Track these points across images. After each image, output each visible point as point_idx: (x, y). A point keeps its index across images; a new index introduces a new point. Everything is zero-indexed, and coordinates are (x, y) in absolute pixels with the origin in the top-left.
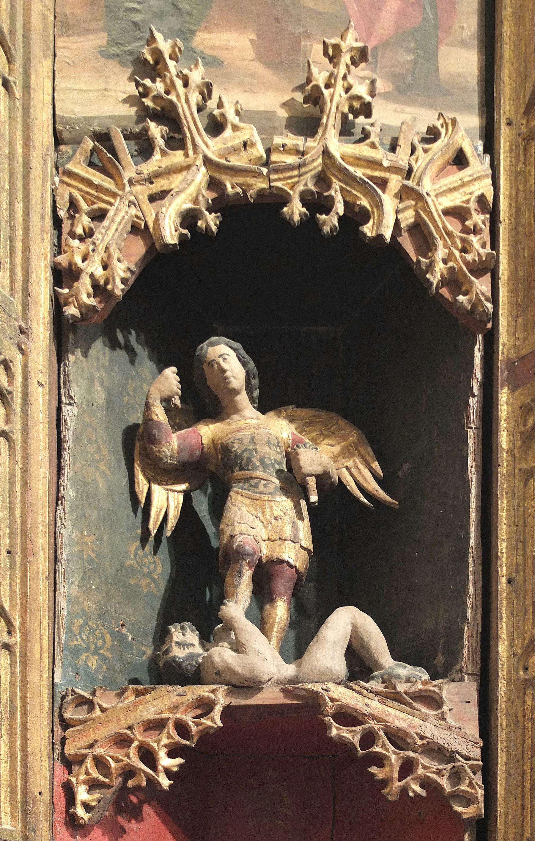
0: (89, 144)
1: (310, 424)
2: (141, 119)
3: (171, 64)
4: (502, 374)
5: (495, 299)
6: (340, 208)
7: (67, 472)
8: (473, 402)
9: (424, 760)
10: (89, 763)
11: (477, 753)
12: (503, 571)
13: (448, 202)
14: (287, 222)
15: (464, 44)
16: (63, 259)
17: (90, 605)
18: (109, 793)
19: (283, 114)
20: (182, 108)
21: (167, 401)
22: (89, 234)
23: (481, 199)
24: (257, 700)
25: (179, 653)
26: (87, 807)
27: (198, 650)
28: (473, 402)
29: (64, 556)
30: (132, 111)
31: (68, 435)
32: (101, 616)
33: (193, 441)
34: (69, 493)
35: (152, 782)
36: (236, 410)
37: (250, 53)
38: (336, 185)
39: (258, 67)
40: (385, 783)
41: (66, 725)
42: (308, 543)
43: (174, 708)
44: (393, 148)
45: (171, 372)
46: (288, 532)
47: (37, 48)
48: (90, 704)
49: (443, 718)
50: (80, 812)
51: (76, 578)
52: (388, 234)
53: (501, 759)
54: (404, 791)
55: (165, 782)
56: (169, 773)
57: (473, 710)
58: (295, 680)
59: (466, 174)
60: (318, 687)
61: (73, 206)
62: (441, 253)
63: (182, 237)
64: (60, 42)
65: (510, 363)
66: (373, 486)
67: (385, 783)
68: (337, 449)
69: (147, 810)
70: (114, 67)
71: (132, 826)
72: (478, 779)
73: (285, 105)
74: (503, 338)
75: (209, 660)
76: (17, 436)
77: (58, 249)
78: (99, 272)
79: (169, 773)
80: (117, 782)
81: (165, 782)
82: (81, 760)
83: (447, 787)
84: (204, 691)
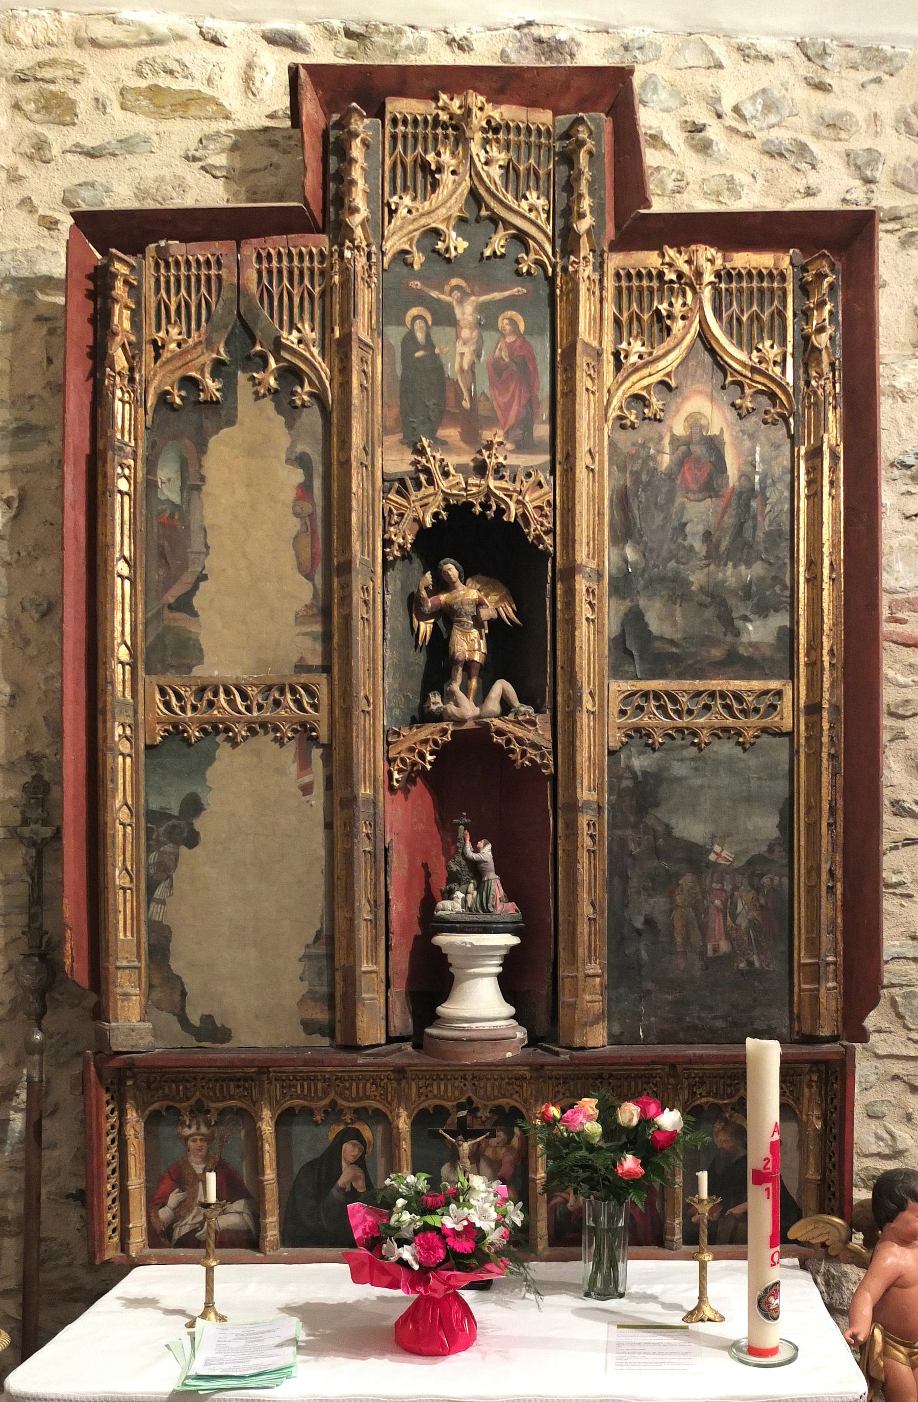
0: (397, 484)
1: (486, 584)
2: (417, 471)
3: (428, 450)
4: (558, 576)
5: (555, 546)
6: (494, 508)
7: (387, 626)
8: (548, 586)
9: (529, 750)
10: (398, 761)
11: (550, 745)
12: (559, 663)
13: (536, 504)
14: (474, 514)
15: (543, 422)
16: (386, 536)
17: (396, 686)
18: (406, 774)
19: (472, 464)
20: (433, 469)
21: (426, 588)
22: (397, 523)
23: (548, 501)
24: (465, 727)
25: (433, 707)
26: (397, 781)
27: (441, 705)
28: (548, 586)
29: (387, 666)
30: (412, 468)
31: (388, 609)
32: (400, 690)
33: (436, 603)
34: (389, 636)
35: (424, 767)
36: (455, 588)
37: (459, 438)
38: (493, 499)
39: (462, 444)
40: (515, 761)
41: (389, 744)
42: (484, 650)
43: (432, 734)
44: (514, 482)
45: (428, 575)
46: (477, 647)
47: (376, 442)
48: (398, 734)
49: (536, 730)
50: (395, 783)
51: (391, 675)
52: (512, 520)
53: (560, 747)
54: (523, 764)
55: (429, 767)
56: (430, 763)
57: (549, 726)
58: (479, 717)
59: (542, 491)
60: (488, 720)
61: (390, 511)
62: (533, 527)
63: (433, 524)
64: (385, 438)
65: (561, 570)
66: (513, 616)
67: (515, 761)
68: (497, 598)
69: (418, 779)
70: (405, 447)
71: (413, 788)
72: (551, 758)
73: (473, 460)
74: (558, 559)
75: (445, 709)
76: (371, 619)
77: (384, 532)
78: (401, 541)
79: (430, 763)
80: (409, 768)
81: (429, 767)
82: (395, 760)
83: (538, 760)
84: (444, 725)
